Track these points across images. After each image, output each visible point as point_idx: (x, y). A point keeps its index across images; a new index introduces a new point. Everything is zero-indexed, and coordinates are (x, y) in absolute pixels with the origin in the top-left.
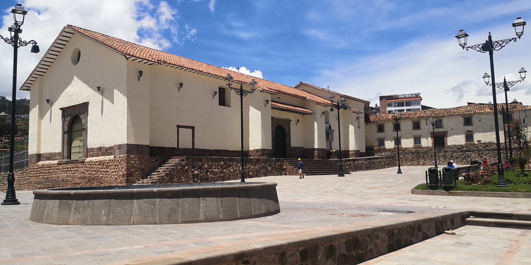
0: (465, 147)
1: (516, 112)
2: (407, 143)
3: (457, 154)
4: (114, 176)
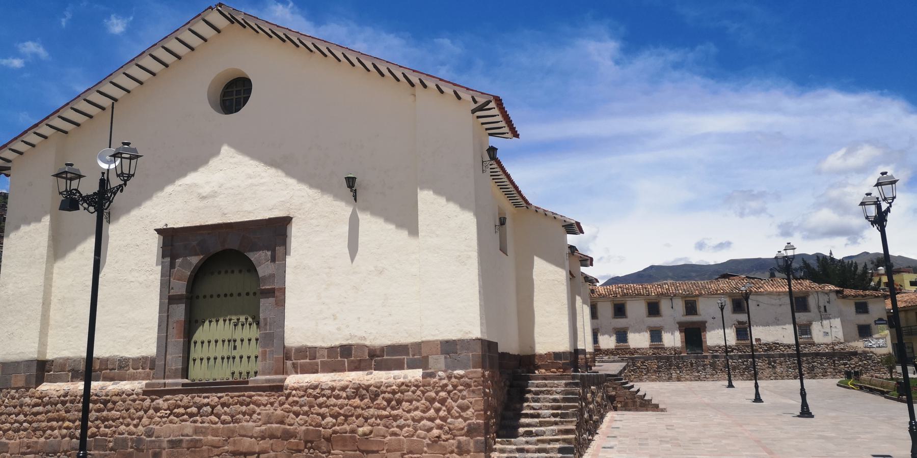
0: (735, 349)
1: (813, 294)
2: (639, 340)
3: (734, 362)
4: (429, 430)
